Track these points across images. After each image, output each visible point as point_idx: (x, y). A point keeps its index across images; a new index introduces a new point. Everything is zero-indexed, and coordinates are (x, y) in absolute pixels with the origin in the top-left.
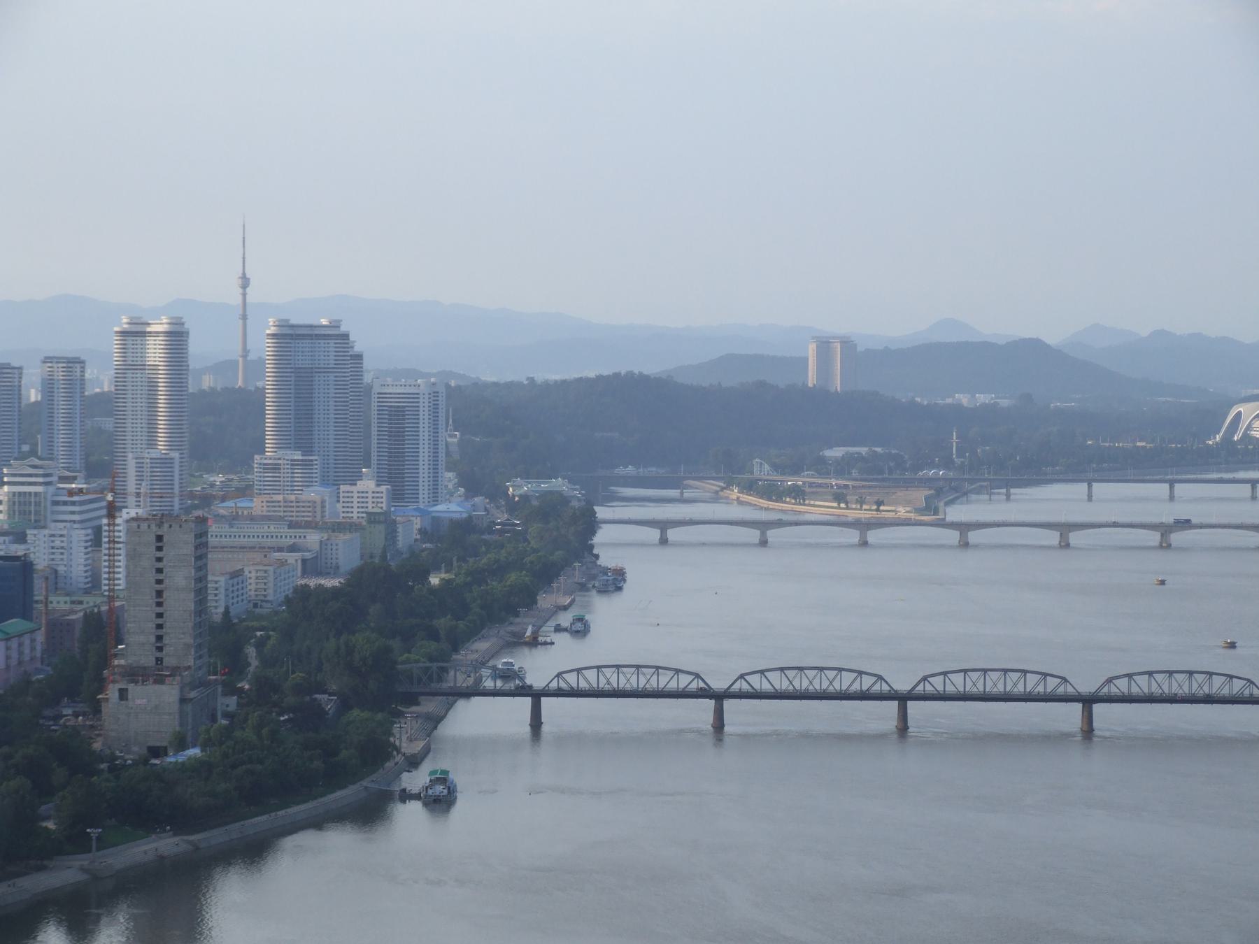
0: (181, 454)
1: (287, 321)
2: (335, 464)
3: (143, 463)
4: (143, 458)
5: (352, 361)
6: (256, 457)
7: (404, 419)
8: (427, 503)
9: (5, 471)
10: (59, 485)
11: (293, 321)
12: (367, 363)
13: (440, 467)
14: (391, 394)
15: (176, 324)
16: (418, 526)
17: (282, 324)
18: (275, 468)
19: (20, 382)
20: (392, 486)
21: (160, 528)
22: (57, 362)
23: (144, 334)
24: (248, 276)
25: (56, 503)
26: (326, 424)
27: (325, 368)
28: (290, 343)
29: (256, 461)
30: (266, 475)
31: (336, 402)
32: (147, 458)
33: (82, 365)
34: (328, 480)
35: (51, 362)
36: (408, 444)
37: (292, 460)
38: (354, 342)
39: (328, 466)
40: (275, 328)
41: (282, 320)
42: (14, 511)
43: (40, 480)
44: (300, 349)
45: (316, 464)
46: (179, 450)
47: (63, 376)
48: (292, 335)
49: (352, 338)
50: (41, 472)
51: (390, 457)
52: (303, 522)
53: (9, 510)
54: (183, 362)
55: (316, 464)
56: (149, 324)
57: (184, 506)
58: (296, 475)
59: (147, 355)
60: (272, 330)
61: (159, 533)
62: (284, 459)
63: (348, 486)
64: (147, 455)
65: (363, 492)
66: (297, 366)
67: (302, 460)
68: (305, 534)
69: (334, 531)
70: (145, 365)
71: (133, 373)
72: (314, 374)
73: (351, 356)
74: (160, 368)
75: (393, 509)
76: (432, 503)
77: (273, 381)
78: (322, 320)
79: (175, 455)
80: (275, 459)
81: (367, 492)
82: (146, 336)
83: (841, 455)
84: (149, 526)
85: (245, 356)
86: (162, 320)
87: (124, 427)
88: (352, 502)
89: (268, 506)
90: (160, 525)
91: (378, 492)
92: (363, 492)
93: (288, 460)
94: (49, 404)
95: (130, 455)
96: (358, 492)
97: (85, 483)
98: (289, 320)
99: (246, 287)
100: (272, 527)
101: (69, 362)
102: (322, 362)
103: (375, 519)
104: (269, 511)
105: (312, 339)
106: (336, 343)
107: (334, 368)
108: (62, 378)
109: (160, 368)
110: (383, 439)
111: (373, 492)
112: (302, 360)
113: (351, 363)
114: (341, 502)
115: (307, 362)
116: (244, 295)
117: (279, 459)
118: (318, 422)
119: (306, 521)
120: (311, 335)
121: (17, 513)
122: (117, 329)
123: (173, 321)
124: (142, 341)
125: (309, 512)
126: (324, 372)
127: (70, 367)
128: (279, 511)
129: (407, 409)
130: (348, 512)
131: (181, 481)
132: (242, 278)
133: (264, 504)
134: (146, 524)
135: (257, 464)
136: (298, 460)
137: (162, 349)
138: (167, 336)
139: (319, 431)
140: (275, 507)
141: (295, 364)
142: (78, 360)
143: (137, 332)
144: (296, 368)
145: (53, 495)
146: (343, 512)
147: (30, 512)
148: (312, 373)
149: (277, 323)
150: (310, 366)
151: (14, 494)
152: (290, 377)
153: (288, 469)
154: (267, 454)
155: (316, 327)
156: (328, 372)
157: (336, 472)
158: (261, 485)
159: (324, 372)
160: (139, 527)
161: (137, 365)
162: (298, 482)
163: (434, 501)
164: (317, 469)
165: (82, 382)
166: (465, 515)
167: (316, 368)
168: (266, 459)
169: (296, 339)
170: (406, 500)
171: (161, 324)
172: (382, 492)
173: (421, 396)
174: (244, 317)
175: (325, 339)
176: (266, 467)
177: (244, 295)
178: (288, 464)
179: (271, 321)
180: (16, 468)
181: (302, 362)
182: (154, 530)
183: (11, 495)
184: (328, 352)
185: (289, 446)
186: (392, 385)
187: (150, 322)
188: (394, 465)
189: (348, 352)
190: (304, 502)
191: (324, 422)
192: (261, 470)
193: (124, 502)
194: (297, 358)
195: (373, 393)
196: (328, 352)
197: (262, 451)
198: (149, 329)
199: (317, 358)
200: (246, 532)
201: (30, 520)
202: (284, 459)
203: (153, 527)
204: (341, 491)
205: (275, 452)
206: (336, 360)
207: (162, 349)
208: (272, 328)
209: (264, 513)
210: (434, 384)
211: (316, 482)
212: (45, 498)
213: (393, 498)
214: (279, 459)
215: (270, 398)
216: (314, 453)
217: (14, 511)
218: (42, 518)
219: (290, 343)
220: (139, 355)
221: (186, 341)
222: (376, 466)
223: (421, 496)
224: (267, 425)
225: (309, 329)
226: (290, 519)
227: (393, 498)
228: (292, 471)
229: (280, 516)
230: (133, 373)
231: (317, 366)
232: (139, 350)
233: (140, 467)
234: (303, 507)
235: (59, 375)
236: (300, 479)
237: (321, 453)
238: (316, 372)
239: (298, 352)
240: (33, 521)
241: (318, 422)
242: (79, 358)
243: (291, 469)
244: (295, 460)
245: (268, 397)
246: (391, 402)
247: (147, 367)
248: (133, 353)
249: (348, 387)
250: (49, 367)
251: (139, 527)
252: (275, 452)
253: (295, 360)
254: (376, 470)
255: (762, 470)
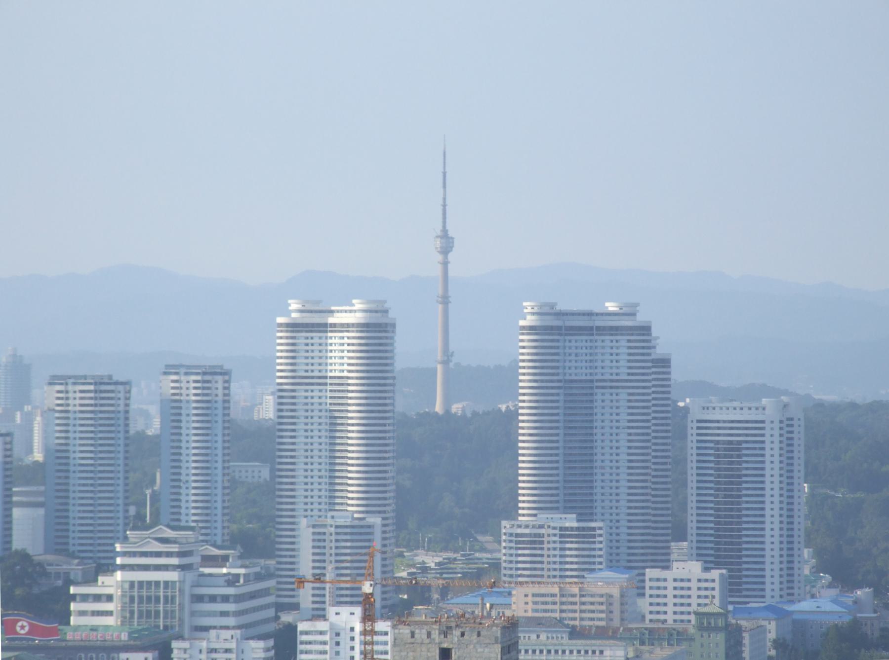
0: (384, 519)
1: (552, 306)
2: (629, 534)
3: (324, 534)
4: (325, 526)
5: (654, 370)
6: (504, 523)
7: (739, 463)
8: (777, 599)
9: (118, 547)
10: (201, 569)
11: (562, 306)
12: (678, 374)
13: (796, 539)
14: (718, 422)
15: (376, 312)
16: (772, 635)
17: (547, 311)
18: (536, 541)
19: (127, 405)
20: (730, 570)
21: (446, 636)
22: (186, 374)
23: (323, 328)
24: (450, 234)
25: (199, 599)
26: (614, 470)
27: (612, 381)
28: (558, 341)
29: (504, 531)
30: (520, 552)
31: (630, 434)
32: (331, 526)
33: (227, 378)
34: (618, 561)
35: (177, 373)
36: (747, 502)
37: (561, 529)
38: (658, 338)
39: (618, 538)
40: (533, 317)
41: (546, 304)
42: (132, 613)
43: (175, 561)
44: (574, 351)
45: (601, 535)
46: (379, 512)
47: (196, 395)
48: (559, 328)
49: (654, 332)
50: (174, 548)
51: (718, 523)
52: (594, 629)
53: (123, 609)
54: (387, 371)
55: (601, 535)
56: (332, 312)
57: (389, 602)
58: (568, 553)
59: (330, 361)
60: (530, 320)
61: (445, 646)
62: (549, 527)
63: (658, 570)
64: (329, 521)
65: (682, 580)
66: (568, 377)
67: (578, 529)
68: (601, 648)
69: (642, 643)
70: (326, 377)
71: (307, 391)
72: (596, 391)
73: (652, 361)
74: (350, 381)
75: (730, 608)
76: (786, 598)
77: (530, 401)
78: (607, 304)
79: (376, 520)
80: (534, 527)
81: (689, 580)
82: (326, 332)
83: (380, 554)
84: (429, 635)
85: (445, 362)
86: (353, 305)
87: (293, 477)
88: (665, 596)
89: (535, 603)
90: (446, 633)
91: (706, 581)
92: (682, 580)
93: (554, 528)
94: (173, 441)
95: (304, 522)
96: (675, 580)
97: (242, 567)
98: (556, 304)
99: (449, 252)
100: (543, 637)
101: (204, 373)
102: (607, 370)
103: (709, 623)
104: (537, 611)
105: (592, 335)
106: (629, 341)
107: (627, 381)
108: (194, 398)
109: (350, 381)
110: (706, 495)
111: (699, 580)
112: (576, 368)
113: (653, 373)
114: (647, 595)
115: (584, 371)
116: (445, 264)
117: (541, 527)
118: (602, 468)
119: (597, 627)
120: (591, 328)
121: (136, 616)
122: (280, 320)
123: (373, 306)
124: (320, 338)
125: (602, 612)
126: (611, 387)
127: (208, 382)
128: (552, 611)
129: (744, 445)
130: (658, 613)
131: (384, 563)
132: (441, 237)
133: (530, 599)
134: (424, 631)
135: (505, 534)
136: (572, 529)
137: (353, 351)
138: (361, 331)
139: (603, 481)
140: (546, 603)
141: (565, 374)
142: (219, 371)
143: (313, 325)
144: (566, 381)
145: (192, 586)
146: (651, 613)
147: (157, 613)
148: (592, 388)
149: (536, 310)
150: (589, 377)
151: (132, 584)
152: (558, 394)
153: (554, 542)
154: (520, 518)
155: (597, 314)
156: (617, 387)
157: (629, 548)
158: (511, 569)
159: (611, 387)
160: (413, 635)
161: (313, 377)
162: (572, 563)
163: (789, 594)
164: (601, 545)
165: (226, 405)
166: (847, 619)
167: (597, 381)
168: (519, 526)
169: (566, 335)
170: (745, 593)
171: (351, 311)
172: (713, 581)
173: (767, 425)
174: (445, 300)
175: (612, 335)
176: (518, 540)
177: (445, 264)
178: (555, 535)
179: (528, 306)
180: (135, 543)
181: (576, 371)
182: (437, 641)
183: (127, 586)
184: (617, 355)
185: (556, 505)
186: (721, 408)
187: (333, 308)
188: (725, 537)
189: (649, 354)
190: (592, 596)
191: (611, 468)
192: (513, 545)
193: (293, 596)
194: (567, 364)
195: (689, 420)
196: (617, 355)
197: (511, 512)
198: (331, 320)
199: (599, 364)
200: (559, 645)
201: (158, 627)
202: (549, 527)
203: (435, 635)
204: (647, 578)
205: (535, 515)
206: (630, 368)
207: (353, 351)
208: (529, 317)
209: (530, 614)
210: (785, 406)
211: (601, 563)
212: (181, 591)
213: (731, 591)
214: (541, 527)
215: (525, 427)
216: (595, 517)
217: (132, 613)
218: (176, 622)
219: (558, 341)
220: (316, 361)
221: (392, 338)
222: (694, 538)
223: (768, 587)
224: (520, 472)
225: (586, 317)
226: (572, 623)
227: (731, 591)
228: (563, 546)
229: (556, 618)
230: (307, 391)
231: (599, 377)
232: (317, 354)
233: (319, 540)
234: (592, 603)
235: (190, 391)
236: (575, 560)
237: (607, 516)
238: (597, 387)
239: (570, 355)
240: (161, 628)
241: (602, 468)
242: (221, 367)
243: (561, 542)
244: (566, 529)
245: (523, 428)
246: (719, 435)
247: (329, 381)
248: (307, 358)
249: (654, 408)
250: (173, 381)
251: (413, 635)
252: (535, 515)
253: (564, 368)
254: (695, 545)
255: (230, 577)
